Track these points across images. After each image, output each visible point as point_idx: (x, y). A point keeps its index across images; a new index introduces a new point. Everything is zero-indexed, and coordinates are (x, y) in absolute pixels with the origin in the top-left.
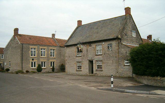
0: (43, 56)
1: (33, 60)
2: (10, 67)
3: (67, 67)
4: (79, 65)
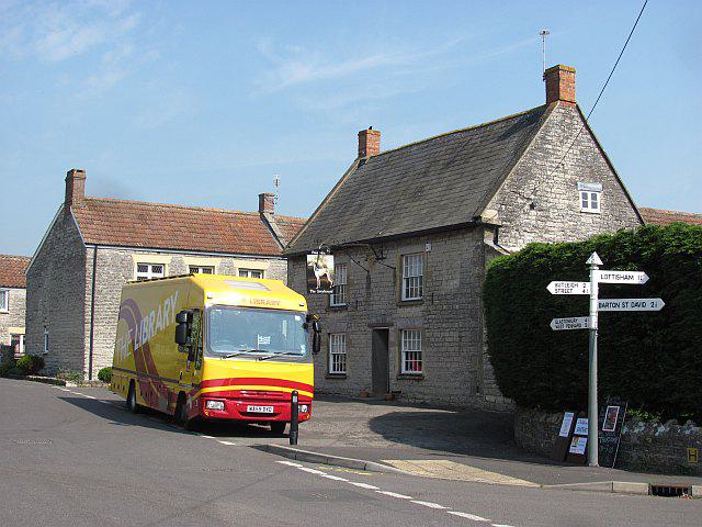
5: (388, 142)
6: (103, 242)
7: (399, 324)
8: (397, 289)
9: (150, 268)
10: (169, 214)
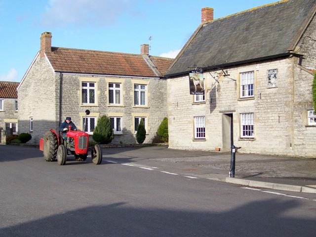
0: (139, 105)
1: (88, 112)
2: (32, 132)
3: (171, 131)
4: (17, 111)
5: (217, 16)
6: (64, 71)
7: (239, 111)
8: (238, 91)
9: (114, 85)
10: (95, 55)
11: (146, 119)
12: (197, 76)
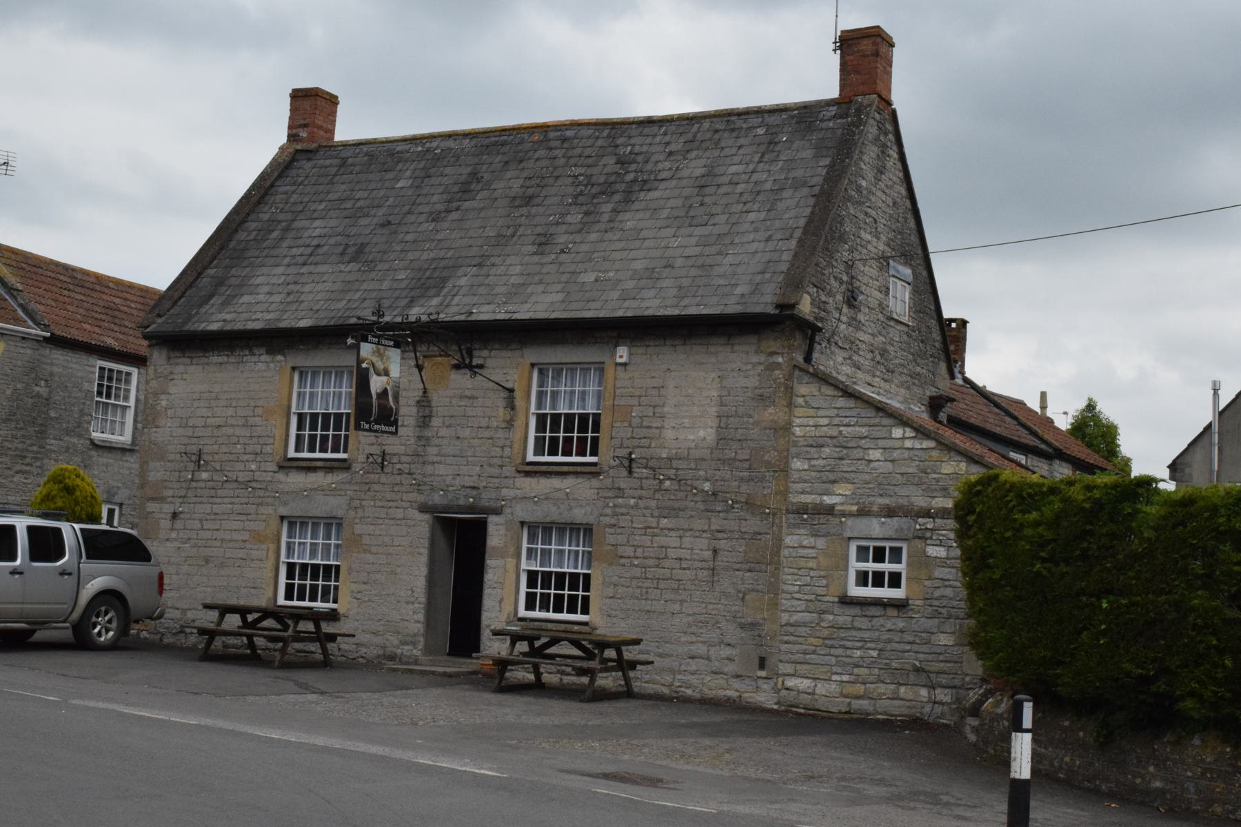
5: (347, 129)
11: (284, 511)
12: (381, 356)
